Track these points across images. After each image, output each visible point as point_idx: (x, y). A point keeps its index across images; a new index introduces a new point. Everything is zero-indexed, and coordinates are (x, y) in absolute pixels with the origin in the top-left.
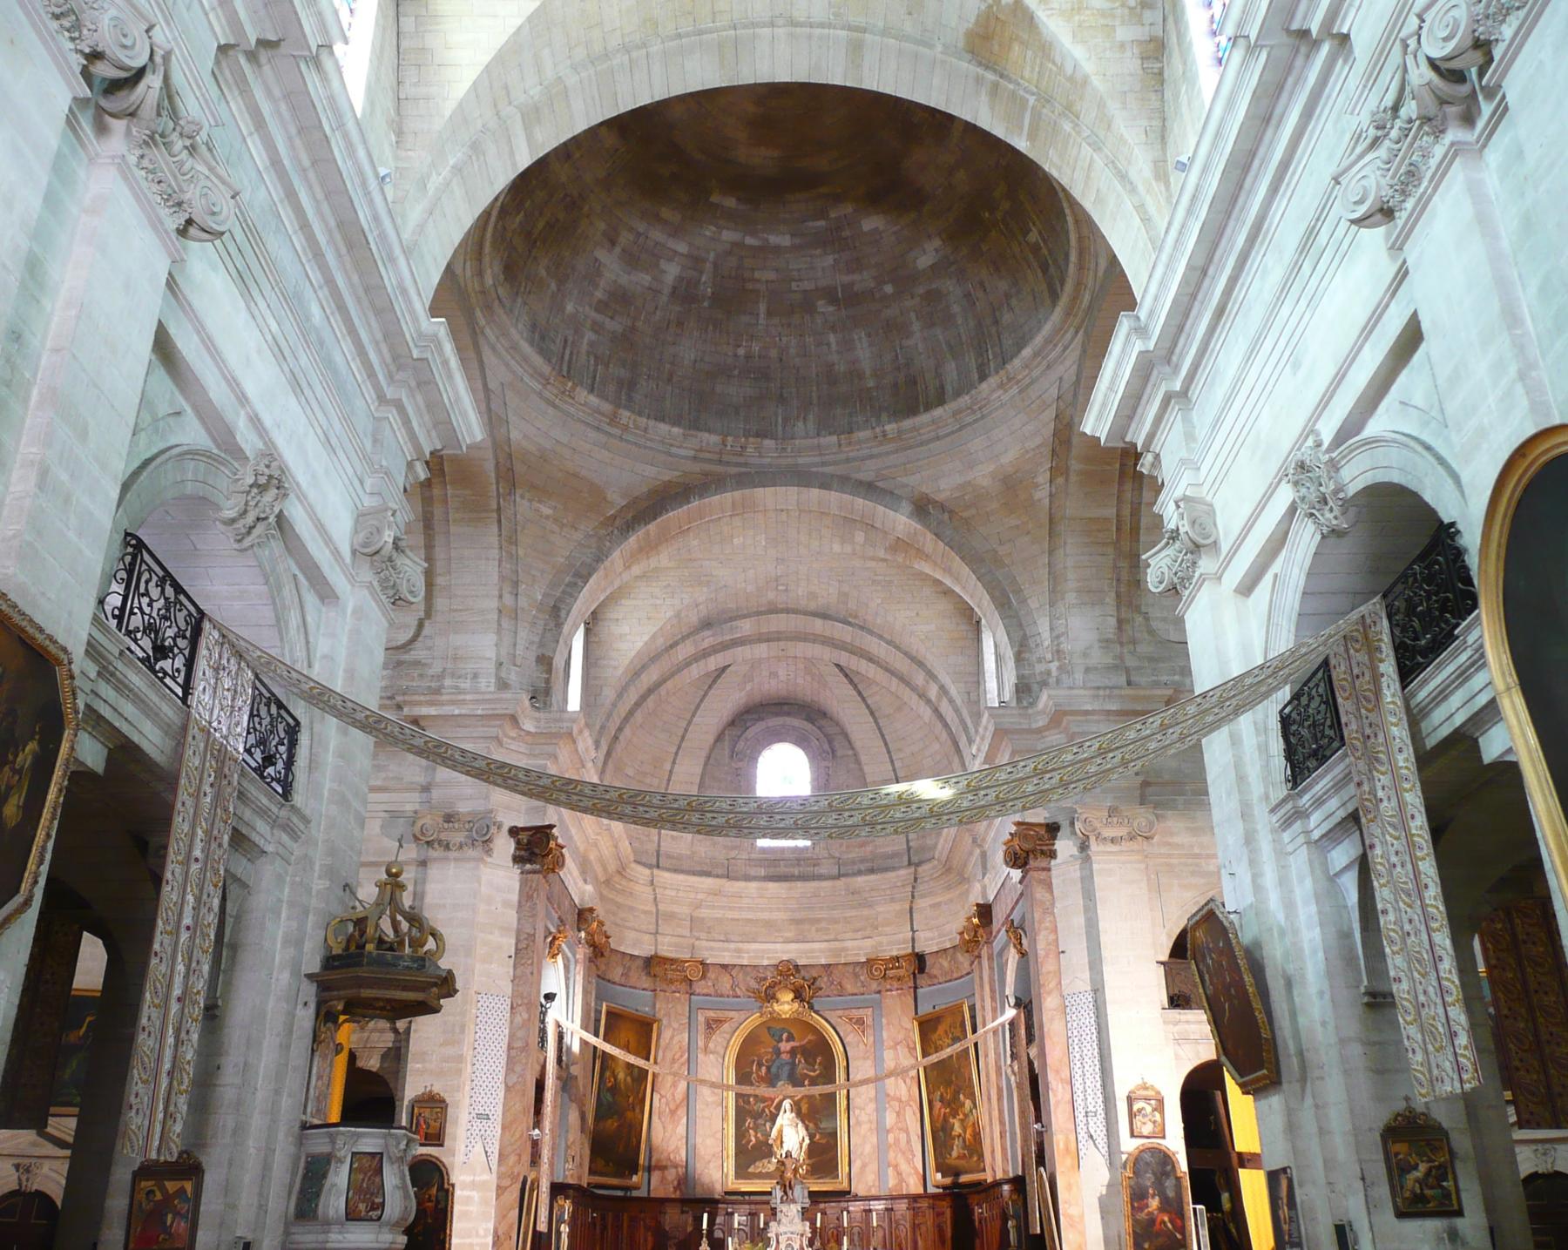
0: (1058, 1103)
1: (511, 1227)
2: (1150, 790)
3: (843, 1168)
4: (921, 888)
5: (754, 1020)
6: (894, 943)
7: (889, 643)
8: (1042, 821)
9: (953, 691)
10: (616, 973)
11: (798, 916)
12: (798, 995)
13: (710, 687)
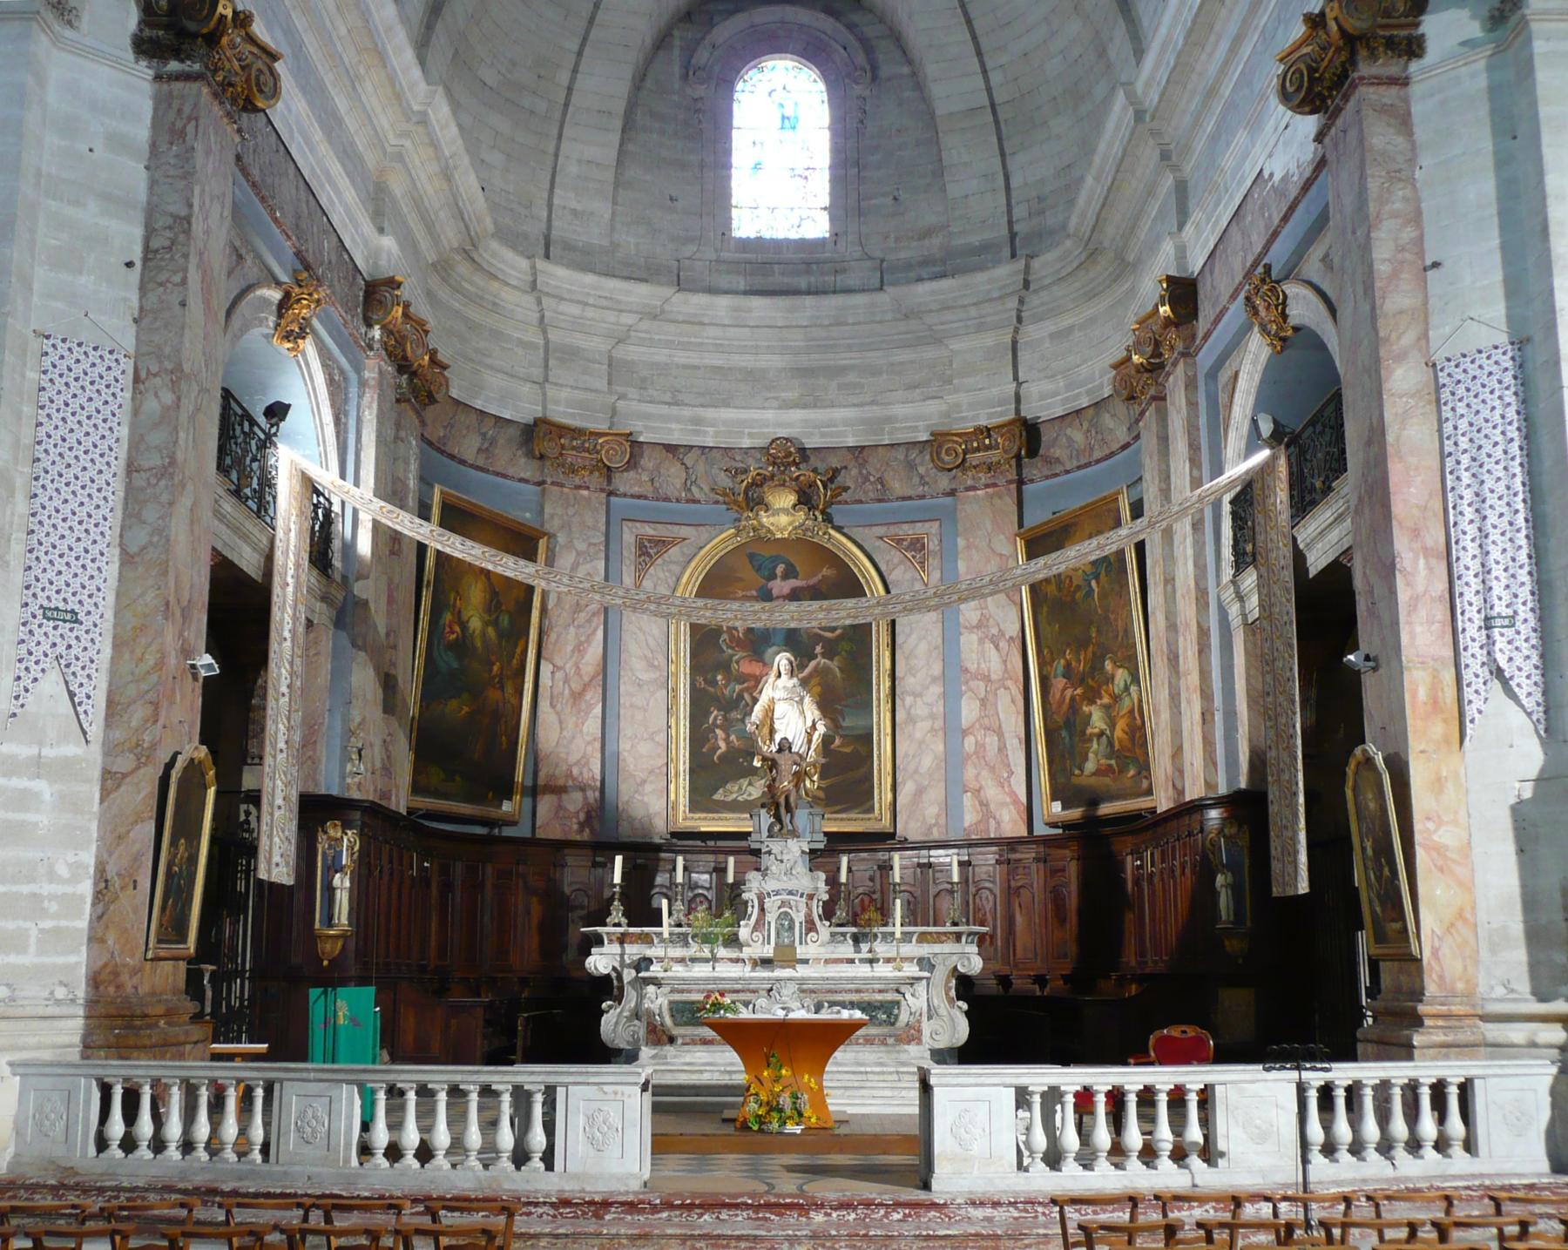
0: (1415, 602)
1: (136, 858)
3: (882, 795)
4: (1034, 301)
5: (721, 541)
6: (980, 403)
10: (469, 447)
12: (805, 499)
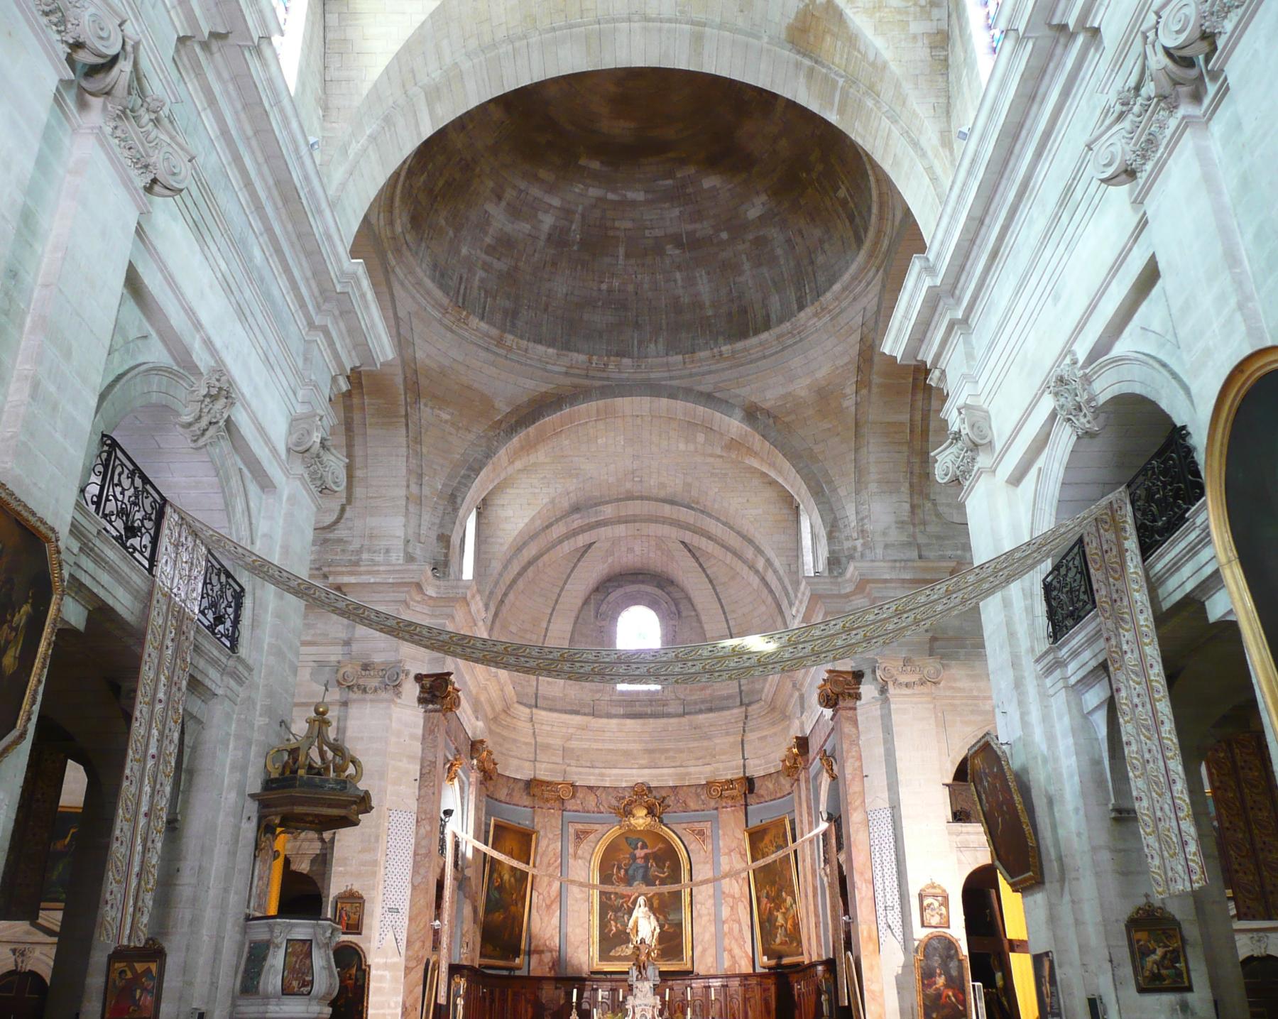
0: (862, 899)
1: (416, 1000)
2: (937, 644)
3: (687, 952)
4: (750, 724)
5: (615, 831)
6: (728, 769)
7: (724, 524)
8: (850, 669)
9: (777, 563)
10: (502, 794)
11: (650, 746)
12: (651, 812)
13: (579, 560)
